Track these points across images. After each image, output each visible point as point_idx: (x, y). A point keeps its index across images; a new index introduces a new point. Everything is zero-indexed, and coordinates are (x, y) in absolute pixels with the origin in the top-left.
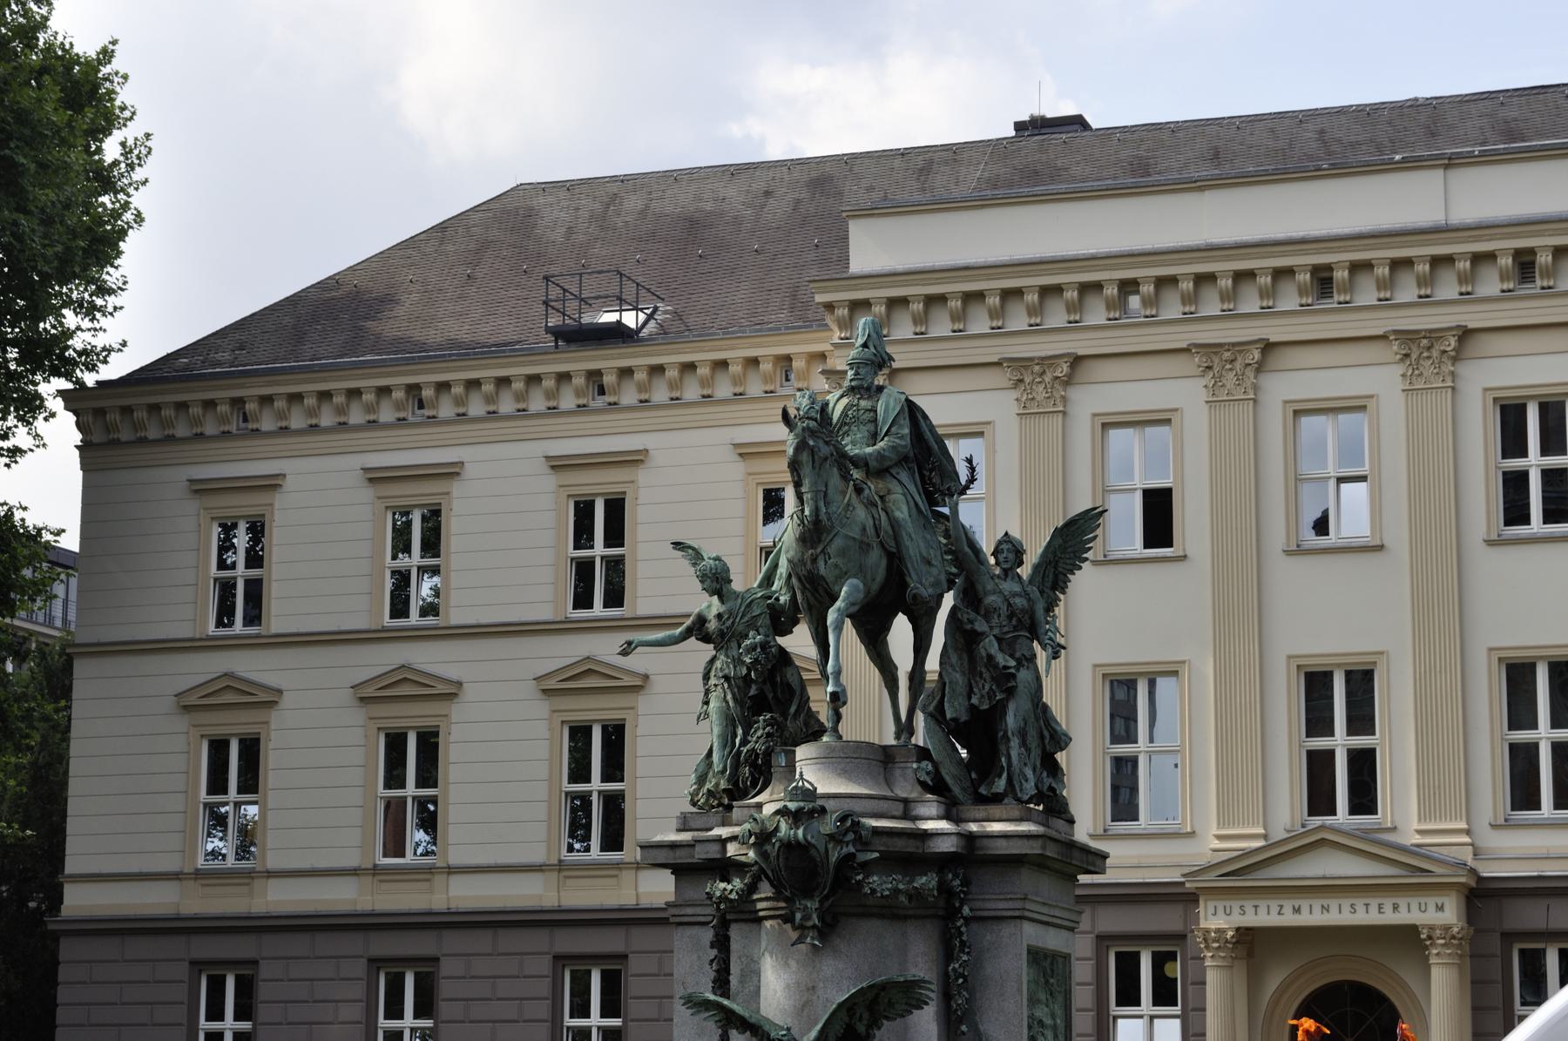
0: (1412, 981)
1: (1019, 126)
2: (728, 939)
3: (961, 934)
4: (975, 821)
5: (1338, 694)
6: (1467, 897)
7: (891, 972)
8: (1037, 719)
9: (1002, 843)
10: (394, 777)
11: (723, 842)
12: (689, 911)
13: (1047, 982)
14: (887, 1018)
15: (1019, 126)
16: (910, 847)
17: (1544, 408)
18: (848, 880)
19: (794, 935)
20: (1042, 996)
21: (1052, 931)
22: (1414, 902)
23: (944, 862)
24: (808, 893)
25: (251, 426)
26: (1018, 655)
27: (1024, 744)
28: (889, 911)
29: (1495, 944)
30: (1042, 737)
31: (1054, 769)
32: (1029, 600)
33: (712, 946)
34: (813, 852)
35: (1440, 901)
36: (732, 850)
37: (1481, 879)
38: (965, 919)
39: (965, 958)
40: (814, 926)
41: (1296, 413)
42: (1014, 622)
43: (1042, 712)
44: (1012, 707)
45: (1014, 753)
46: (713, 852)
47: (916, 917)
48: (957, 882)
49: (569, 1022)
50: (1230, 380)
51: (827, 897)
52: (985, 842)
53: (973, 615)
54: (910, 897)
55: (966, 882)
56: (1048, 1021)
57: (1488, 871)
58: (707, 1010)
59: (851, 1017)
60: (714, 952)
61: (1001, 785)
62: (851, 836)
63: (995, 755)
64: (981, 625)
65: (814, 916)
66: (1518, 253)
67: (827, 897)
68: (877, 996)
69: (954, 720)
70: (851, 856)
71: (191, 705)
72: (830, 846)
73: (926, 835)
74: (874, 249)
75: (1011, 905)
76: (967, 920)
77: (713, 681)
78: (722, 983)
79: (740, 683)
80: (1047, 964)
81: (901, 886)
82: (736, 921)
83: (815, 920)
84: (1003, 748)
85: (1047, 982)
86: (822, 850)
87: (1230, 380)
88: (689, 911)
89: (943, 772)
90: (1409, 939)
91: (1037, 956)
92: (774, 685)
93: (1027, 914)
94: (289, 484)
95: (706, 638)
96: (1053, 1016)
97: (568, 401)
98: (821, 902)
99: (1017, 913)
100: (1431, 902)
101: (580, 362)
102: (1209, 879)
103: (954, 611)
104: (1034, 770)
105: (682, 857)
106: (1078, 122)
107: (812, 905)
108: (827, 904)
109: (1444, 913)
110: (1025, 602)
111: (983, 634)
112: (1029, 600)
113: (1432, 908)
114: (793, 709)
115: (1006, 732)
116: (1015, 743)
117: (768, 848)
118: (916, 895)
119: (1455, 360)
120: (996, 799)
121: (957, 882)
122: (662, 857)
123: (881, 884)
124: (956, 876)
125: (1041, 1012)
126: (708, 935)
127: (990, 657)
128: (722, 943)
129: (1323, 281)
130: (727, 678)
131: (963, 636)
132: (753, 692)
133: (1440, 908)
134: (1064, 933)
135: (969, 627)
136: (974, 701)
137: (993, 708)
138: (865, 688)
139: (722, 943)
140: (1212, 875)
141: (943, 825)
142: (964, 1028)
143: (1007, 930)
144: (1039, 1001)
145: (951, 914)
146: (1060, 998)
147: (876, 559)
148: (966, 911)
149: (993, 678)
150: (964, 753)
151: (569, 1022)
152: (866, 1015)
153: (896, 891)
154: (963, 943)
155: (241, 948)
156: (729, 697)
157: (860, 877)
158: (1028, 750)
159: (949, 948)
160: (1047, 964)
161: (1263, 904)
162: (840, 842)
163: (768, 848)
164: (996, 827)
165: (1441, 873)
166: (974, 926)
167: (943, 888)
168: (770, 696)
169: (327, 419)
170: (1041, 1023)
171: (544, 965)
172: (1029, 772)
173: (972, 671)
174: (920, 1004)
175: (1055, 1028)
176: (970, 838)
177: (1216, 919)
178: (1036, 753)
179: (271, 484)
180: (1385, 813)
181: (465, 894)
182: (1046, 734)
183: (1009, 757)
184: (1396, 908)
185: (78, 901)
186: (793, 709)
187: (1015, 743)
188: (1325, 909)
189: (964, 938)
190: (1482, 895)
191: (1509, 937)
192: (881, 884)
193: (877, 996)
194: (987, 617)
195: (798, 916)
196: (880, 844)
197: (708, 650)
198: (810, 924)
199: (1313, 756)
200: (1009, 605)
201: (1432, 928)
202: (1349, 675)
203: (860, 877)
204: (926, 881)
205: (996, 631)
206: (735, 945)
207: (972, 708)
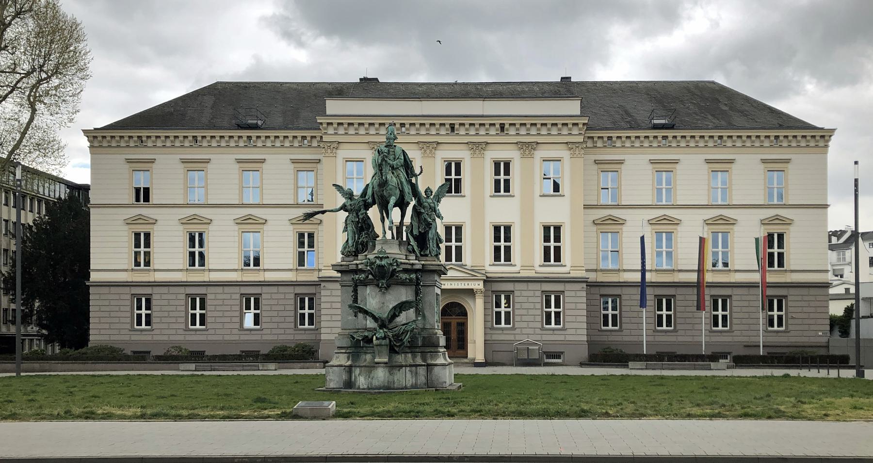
1: (361, 79)
5: (551, 233)
10: (138, 245)
11: (357, 265)
15: (361, 79)
17: (505, 164)
23: (416, 271)
28: (403, 283)
36: (360, 267)
46: (354, 267)
49: (545, 310)
50: (428, 151)
57: (489, 275)
64: (423, 211)
66: (501, 124)
71: (129, 222)
74: (333, 106)
87: (428, 151)
90: (471, 293)
95: (346, 211)
97: (187, 144)
101: (245, 133)
103: (414, 206)
105: (343, 268)
106: (376, 79)
109: (478, 286)
118: (411, 280)
120: (426, 255)
122: (339, 268)
126: (352, 289)
128: (355, 291)
129: (452, 127)
131: (416, 212)
138: (386, 224)
139: (355, 291)
141: (417, 262)
143: (431, 288)
145: (418, 284)
147: (398, 192)
151: (545, 310)
155: (509, 287)
167: (417, 278)
169: (123, 144)
171: (183, 297)
173: (419, 222)
180: (463, 262)
181: (160, 277)
185: (94, 277)
190: (487, 281)
192: (404, 276)
194: (424, 208)
197: (347, 214)
199: (136, 253)
202: (145, 234)
204: (413, 276)
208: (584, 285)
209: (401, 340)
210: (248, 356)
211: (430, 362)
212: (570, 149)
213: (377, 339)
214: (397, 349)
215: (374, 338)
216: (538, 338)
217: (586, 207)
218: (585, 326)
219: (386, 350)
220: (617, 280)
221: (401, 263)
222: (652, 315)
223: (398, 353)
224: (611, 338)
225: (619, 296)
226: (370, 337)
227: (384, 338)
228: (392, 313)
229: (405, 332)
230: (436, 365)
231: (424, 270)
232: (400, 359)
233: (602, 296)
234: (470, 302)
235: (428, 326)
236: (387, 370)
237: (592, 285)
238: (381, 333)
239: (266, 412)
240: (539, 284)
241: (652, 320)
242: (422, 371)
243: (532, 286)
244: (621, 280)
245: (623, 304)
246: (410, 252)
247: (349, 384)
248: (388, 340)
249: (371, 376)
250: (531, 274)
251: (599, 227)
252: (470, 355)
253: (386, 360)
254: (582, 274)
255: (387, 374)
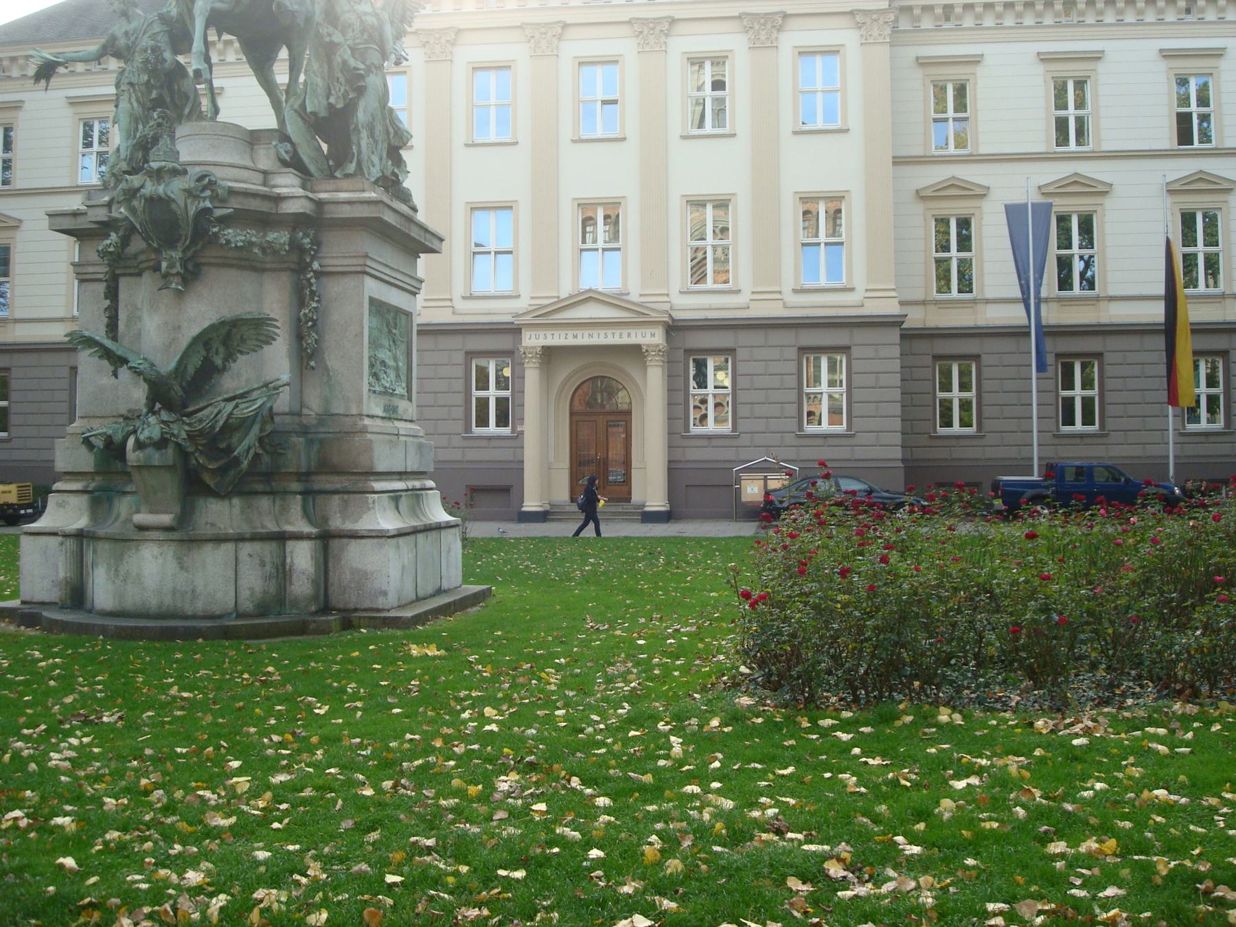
0: (635, 374)
2: (117, 288)
3: (311, 285)
4: (326, 192)
6: (667, 332)
7: (246, 309)
8: (384, 119)
9: (347, 208)
12: (91, 269)
13: (390, 332)
14: (241, 353)
16: (265, 207)
18: (207, 231)
19: (161, 283)
20: (386, 343)
21: (394, 290)
22: (639, 332)
23: (299, 221)
24: (171, 244)
25: (7, 74)
26: (368, 63)
27: (372, 135)
28: (247, 262)
29: (680, 355)
30: (388, 133)
31: (399, 162)
32: (379, 19)
33: (106, 298)
34: (174, 206)
35: (653, 331)
37: (673, 320)
38: (315, 272)
39: (314, 305)
40: (178, 274)
41: (580, 64)
42: (366, 37)
43: (389, 115)
44: (362, 105)
45: (364, 143)
47: (273, 270)
48: (308, 240)
51: (188, 248)
52: (332, 207)
53: (331, 29)
54: (263, 250)
55: (317, 243)
56: (391, 363)
57: (678, 315)
58: (90, 347)
59: (208, 350)
60: (108, 302)
61: (352, 168)
62: (208, 193)
63: (348, 145)
64: (337, 38)
65: (178, 265)
67: (188, 248)
68: (229, 334)
69: (314, 114)
70: (207, 211)
72: (189, 201)
73: (279, 199)
75: (355, 261)
76: (319, 275)
77: (123, 88)
78: (112, 327)
79: (143, 88)
80: (390, 317)
81: (254, 239)
82: (124, 275)
83: (178, 268)
84: (354, 138)
85: (390, 332)
86: (182, 205)
88: (91, 269)
89: (300, 152)
90: (635, 352)
91: (378, 307)
92: (171, 92)
93: (368, 270)
94: (26, 106)
96: (395, 359)
98: (183, 252)
99: (359, 269)
100: (648, 331)
102: (527, 319)
104: (381, 159)
105: (81, 223)
107: (176, 255)
108: (189, 254)
109: (653, 338)
110: (375, 20)
111: (338, 44)
112: (379, 19)
113: (648, 335)
114: (187, 111)
115: (357, 126)
116: (364, 134)
117: (135, 203)
118: (267, 248)
119: (667, 35)
121: (308, 240)
122: (68, 223)
123: (235, 236)
124: (306, 235)
125: (383, 355)
126: (101, 288)
127: (345, 62)
130: (131, 84)
132: (154, 95)
133: (653, 335)
134: (407, 295)
135: (327, 39)
136: (332, 100)
137: (347, 106)
139: (112, 294)
140: (528, 317)
142: (312, 363)
143: (348, 283)
144: (382, 346)
145: (301, 269)
146: (403, 347)
148: (316, 266)
149: (347, 81)
150: (325, 147)
152: (222, 350)
153: (252, 244)
154: (313, 293)
156: (133, 100)
157: (215, 230)
158: (376, 142)
159: (302, 295)
160: (390, 317)
161: (556, 333)
162: (196, 197)
163: (135, 203)
164: (343, 196)
165: (654, 316)
166: (324, 280)
167: (295, 246)
168: (168, 100)
170: (383, 363)
172: (375, 159)
174: (269, 340)
175: (397, 369)
176: (320, 204)
177: (533, 340)
178: (383, 148)
179: (17, 106)
182: (391, 130)
183: (359, 146)
184: (629, 335)
186: (187, 111)
187: (364, 134)
188: (591, 336)
189: (314, 288)
190: (674, 328)
191: (689, 352)
193: (229, 334)
195: (164, 265)
196: (235, 203)
198: (174, 271)
200: (361, 21)
201: (648, 346)
203: (215, 230)
204: (279, 237)
205: (350, 42)
206: (123, 296)
207: (330, 106)
208: (894, 335)
209: (229, 450)
210: (1215, 485)
211: (336, 523)
212: (859, 26)
213: (140, 445)
214: (207, 478)
215: (131, 442)
216: (791, 453)
217: (898, 161)
218: (897, 424)
219: (170, 486)
220: (971, 323)
221: (232, 192)
222: (1050, 398)
223: (210, 492)
224: (958, 453)
225: (976, 358)
226: (118, 438)
227: (161, 443)
228: (195, 362)
229: (244, 424)
230: (355, 536)
231: (316, 222)
232: (220, 514)
233: (936, 358)
234: (635, 374)
235: (338, 408)
236: (170, 551)
237: (911, 336)
238: (152, 429)
239: (209, 624)
240: (792, 333)
241: (1050, 411)
242: (302, 556)
243: (776, 337)
244: (981, 323)
245: (985, 374)
246: (284, 163)
247: (77, 595)
248: (170, 451)
249: (123, 569)
250: (773, 310)
251: (931, 204)
252: (636, 497)
253: (166, 519)
254: (890, 308)
255: (172, 566)
